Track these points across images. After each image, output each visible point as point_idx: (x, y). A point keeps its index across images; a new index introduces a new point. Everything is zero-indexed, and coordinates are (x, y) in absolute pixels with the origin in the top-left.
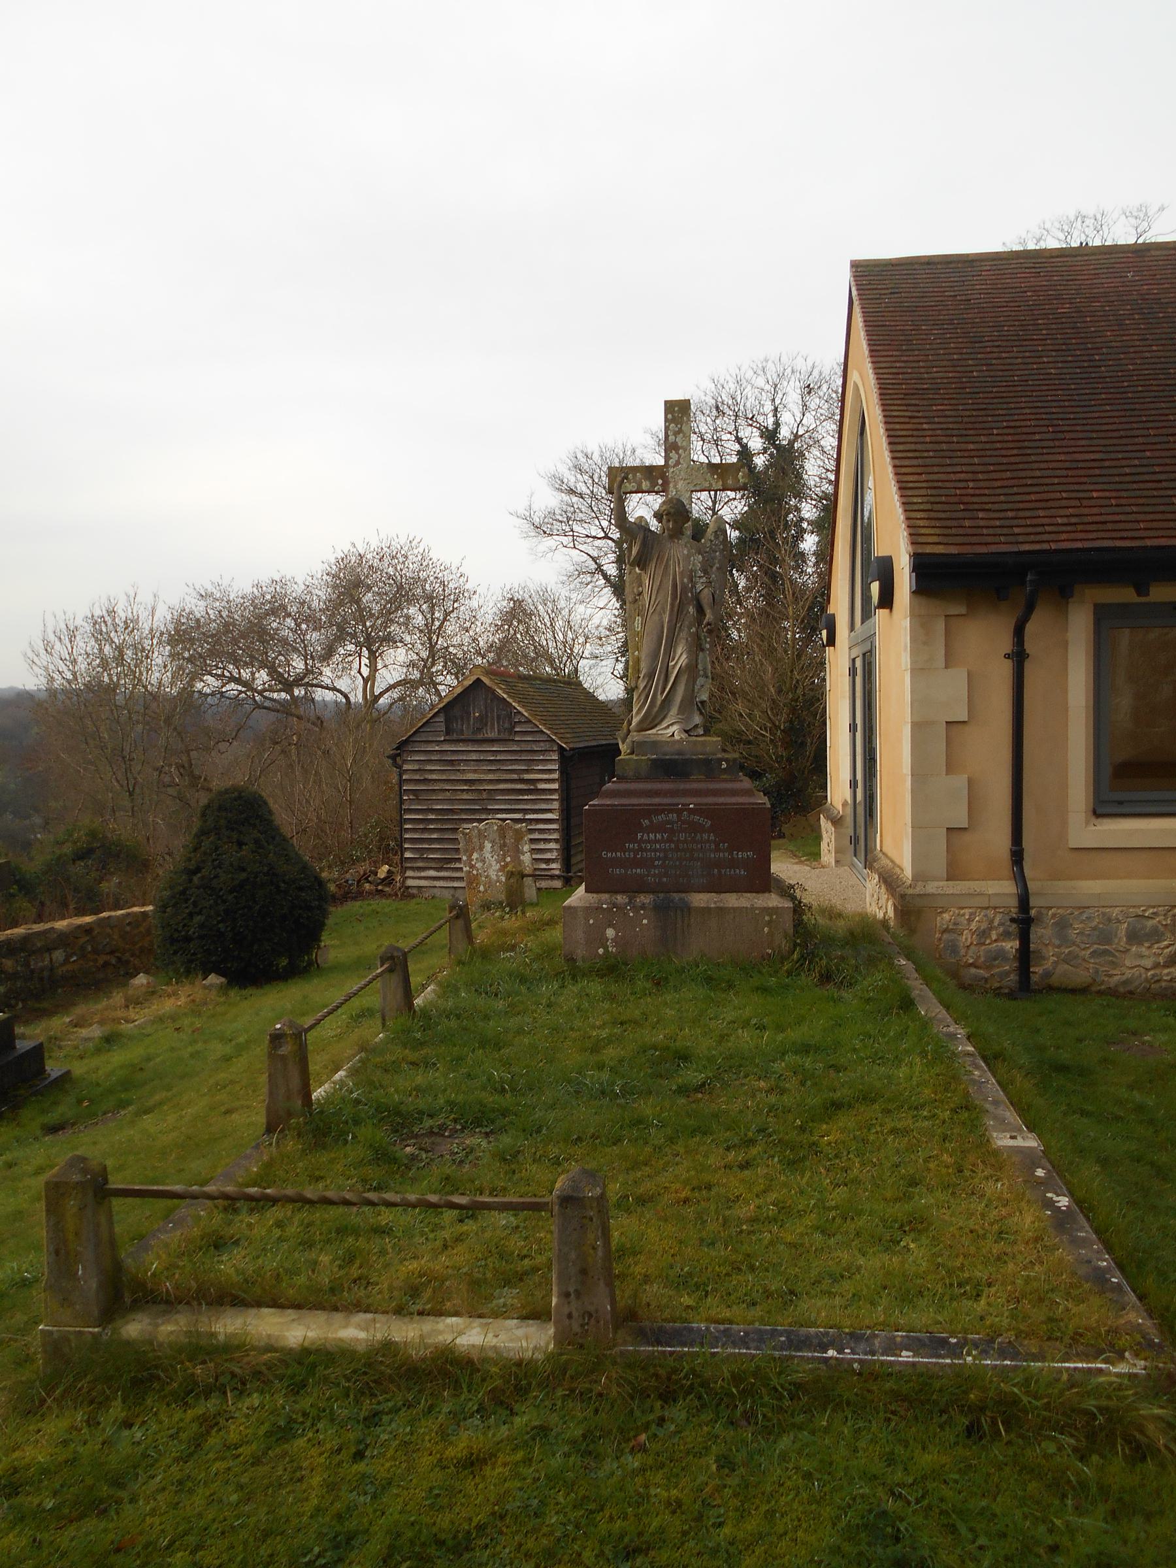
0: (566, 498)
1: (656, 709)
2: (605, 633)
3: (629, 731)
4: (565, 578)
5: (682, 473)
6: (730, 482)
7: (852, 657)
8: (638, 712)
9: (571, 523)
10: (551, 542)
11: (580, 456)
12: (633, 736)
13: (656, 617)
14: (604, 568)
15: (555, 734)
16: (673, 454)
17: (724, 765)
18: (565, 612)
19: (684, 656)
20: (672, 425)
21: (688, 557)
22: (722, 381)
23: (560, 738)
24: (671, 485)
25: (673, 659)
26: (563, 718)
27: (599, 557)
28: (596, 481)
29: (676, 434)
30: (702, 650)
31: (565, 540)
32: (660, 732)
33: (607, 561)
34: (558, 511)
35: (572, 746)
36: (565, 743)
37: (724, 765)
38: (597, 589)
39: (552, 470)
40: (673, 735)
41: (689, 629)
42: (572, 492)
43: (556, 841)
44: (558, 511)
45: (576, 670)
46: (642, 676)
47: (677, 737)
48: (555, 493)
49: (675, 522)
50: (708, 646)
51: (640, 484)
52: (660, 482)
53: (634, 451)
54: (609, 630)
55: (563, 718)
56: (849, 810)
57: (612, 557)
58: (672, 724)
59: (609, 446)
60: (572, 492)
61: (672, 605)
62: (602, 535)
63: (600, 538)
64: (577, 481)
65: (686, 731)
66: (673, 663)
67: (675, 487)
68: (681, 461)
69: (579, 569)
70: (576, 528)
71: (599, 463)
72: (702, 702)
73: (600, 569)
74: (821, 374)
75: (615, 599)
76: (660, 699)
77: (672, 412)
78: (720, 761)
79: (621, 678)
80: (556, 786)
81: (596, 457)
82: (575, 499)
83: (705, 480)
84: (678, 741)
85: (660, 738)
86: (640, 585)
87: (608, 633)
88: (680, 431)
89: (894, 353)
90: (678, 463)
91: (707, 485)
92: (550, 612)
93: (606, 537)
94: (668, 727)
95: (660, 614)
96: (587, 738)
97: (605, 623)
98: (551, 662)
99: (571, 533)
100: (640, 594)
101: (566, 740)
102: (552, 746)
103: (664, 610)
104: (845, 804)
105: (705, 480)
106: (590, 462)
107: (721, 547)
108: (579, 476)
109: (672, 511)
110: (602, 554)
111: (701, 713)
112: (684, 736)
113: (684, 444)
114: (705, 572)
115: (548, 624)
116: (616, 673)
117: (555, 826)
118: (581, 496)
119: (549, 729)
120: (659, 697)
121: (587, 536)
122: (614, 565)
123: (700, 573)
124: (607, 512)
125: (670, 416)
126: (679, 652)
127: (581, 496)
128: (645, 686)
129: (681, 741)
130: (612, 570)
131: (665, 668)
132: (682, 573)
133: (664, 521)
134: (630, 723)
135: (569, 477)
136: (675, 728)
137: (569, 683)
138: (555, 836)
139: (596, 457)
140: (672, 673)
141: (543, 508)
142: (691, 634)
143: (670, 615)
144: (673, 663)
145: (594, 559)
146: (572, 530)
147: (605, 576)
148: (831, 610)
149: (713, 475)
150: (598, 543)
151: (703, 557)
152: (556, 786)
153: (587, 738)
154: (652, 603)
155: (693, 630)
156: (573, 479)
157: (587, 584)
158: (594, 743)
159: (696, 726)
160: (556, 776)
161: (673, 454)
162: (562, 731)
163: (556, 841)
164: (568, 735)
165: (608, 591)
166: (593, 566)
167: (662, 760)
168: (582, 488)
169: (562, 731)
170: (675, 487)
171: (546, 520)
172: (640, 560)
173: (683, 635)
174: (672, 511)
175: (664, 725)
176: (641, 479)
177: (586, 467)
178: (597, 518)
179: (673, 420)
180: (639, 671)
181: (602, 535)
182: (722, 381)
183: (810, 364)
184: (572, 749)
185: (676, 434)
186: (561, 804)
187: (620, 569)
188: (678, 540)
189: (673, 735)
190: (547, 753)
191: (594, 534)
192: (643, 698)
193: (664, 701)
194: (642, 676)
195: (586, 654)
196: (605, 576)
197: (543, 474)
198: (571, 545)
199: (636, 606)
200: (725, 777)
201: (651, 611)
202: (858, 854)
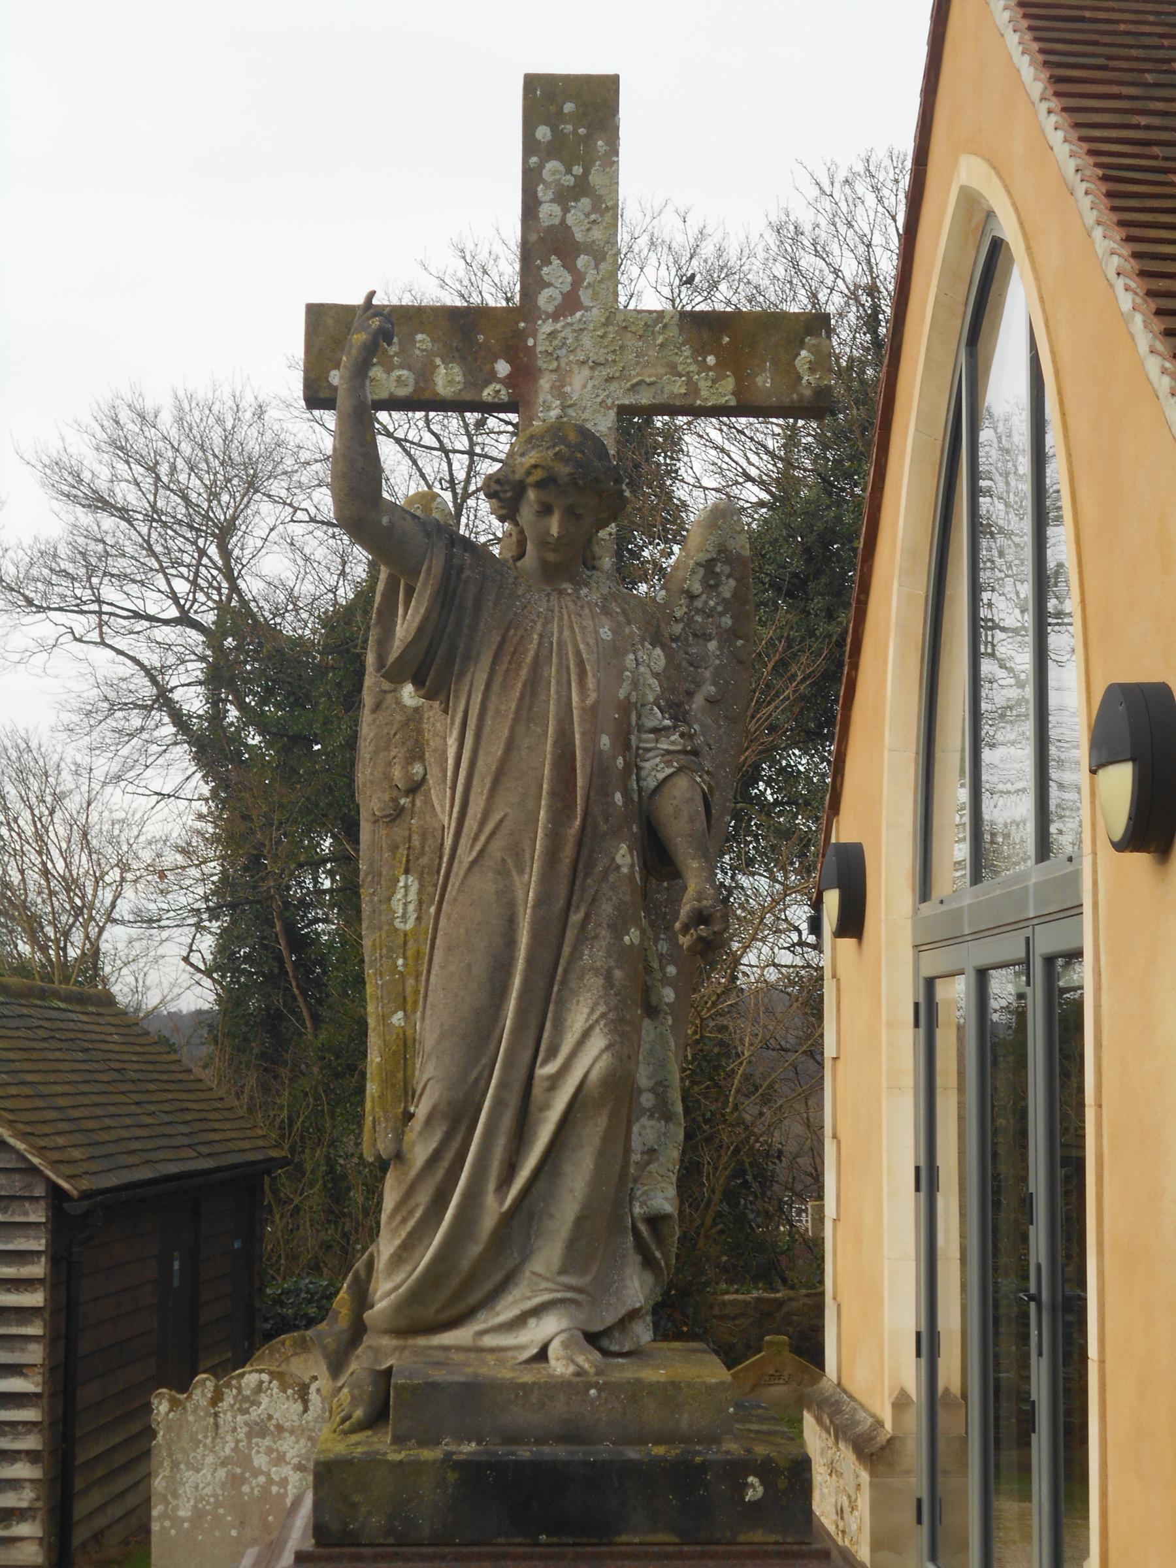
0: (85, 518)
1: (475, 1249)
2: (173, 858)
3: (358, 1330)
4: (75, 718)
5: (587, 341)
6: (765, 381)
7: (927, 972)
8: (398, 1259)
9: (95, 580)
10: (42, 627)
11: (125, 416)
12: (377, 1351)
13: (486, 884)
14: (176, 695)
15: (41, 1151)
16: (554, 271)
17: (755, 1490)
18: (73, 804)
19: (598, 1042)
20: (553, 165)
21: (616, 650)
22: (483, 256)
23: (54, 1164)
24: (545, 383)
25: (553, 1052)
26: (61, 1102)
27: (163, 669)
28: (165, 479)
29: (565, 197)
30: (652, 1011)
31: (80, 624)
32: (489, 1341)
33: (185, 679)
34: (63, 551)
35: (85, 1184)
36: (69, 1178)
37: (755, 1490)
38: (154, 748)
39: (54, 449)
40: (542, 1355)
41: (618, 930)
42: (100, 503)
43: (32, 1456)
44: (63, 551)
45: (96, 952)
46: (421, 1110)
47: (559, 1366)
48: (60, 506)
49: (571, 513)
50: (669, 994)
51: (425, 375)
52: (503, 368)
53: (260, 412)
54: (183, 851)
55: (61, 1102)
56: (915, 1423)
57: (196, 669)
58: (537, 1311)
59: (200, 396)
60: (100, 503)
61: (555, 837)
62: (173, 613)
63: (166, 622)
64: (114, 478)
65: (593, 1339)
66: (551, 1068)
67: (558, 390)
68: (585, 297)
69: (112, 695)
70: (109, 593)
71: (174, 434)
72: (655, 1221)
73: (164, 699)
74: (720, 251)
75: (199, 775)
76: (493, 1209)
77: (554, 120)
78: (737, 1470)
79: (208, 973)
80: (36, 1299)
81: (166, 421)
82: (108, 522)
83: (673, 370)
84: (565, 1386)
85: (488, 1369)
86: (416, 754)
87: (180, 859)
88: (582, 188)
89: (1125, 90)
90: (570, 303)
91: (678, 387)
92: (33, 800)
93: (185, 620)
94: (520, 1321)
95: (503, 872)
96: (131, 1160)
97: (177, 833)
98: (33, 927)
99: (95, 607)
100: (415, 787)
101: (68, 1170)
102: (29, 1186)
103: (517, 853)
104: (901, 1403)
105: (673, 370)
106: (151, 433)
107: (727, 621)
108: (121, 467)
109: (564, 470)
110: (171, 660)
111: (649, 1262)
112: (587, 1360)
113: (596, 234)
114: (677, 711)
115: (29, 830)
116: (195, 958)
117: (29, 1414)
118: (124, 513)
119: (24, 1136)
120: (490, 1200)
121: (137, 615)
122: (199, 689)
123: (658, 718)
124: (187, 559)
125: (543, 133)
126: (579, 1017)
127: (124, 513)
128: (434, 1159)
129: (575, 1387)
130: (193, 701)
131: (517, 1086)
132: (592, 712)
133: (527, 514)
134: (362, 1301)
135: (97, 467)
136: (549, 1327)
137: (81, 999)
138: (31, 1442)
139: (166, 421)
140: (546, 1106)
141: (27, 541)
142: (622, 954)
143: (547, 877)
144: (551, 1068)
145: (148, 672)
146: (99, 601)
147: (179, 718)
148: (845, 831)
149: (700, 351)
150: (164, 633)
151: (669, 656)
152: (36, 1299)
153: (131, 1160)
154: (471, 824)
155: (632, 937)
156: (105, 473)
157: (132, 735)
158: (145, 1174)
159: (633, 1315)
160: (37, 1270)
161: (554, 271)
162: (60, 1141)
163: (32, 1456)
164: (77, 1154)
165: (182, 754)
166: (147, 690)
167: (499, 1467)
168: (127, 495)
169: (60, 1141)
170: (558, 390)
171: (34, 572)
172: (429, 655)
173: (595, 955)
174: (564, 470)
175: (507, 1309)
176: (429, 355)
177: (139, 444)
178: (162, 570)
179: (557, 149)
180: (408, 1093)
181: (173, 613)
182: (483, 256)
183: (693, 231)
184: (87, 1195)
185: (565, 197)
186: (50, 1353)
187: (215, 701)
188: (579, 583)
189: (542, 1355)
190: (14, 1205)
191: (152, 610)
192: (423, 1198)
193: (508, 1219)
194: (421, 1110)
195: (123, 909)
196: (179, 718)
197: (29, 456)
198: (94, 636)
199: (399, 832)
200: (758, 1536)
201: (466, 856)
202: (941, 1552)
